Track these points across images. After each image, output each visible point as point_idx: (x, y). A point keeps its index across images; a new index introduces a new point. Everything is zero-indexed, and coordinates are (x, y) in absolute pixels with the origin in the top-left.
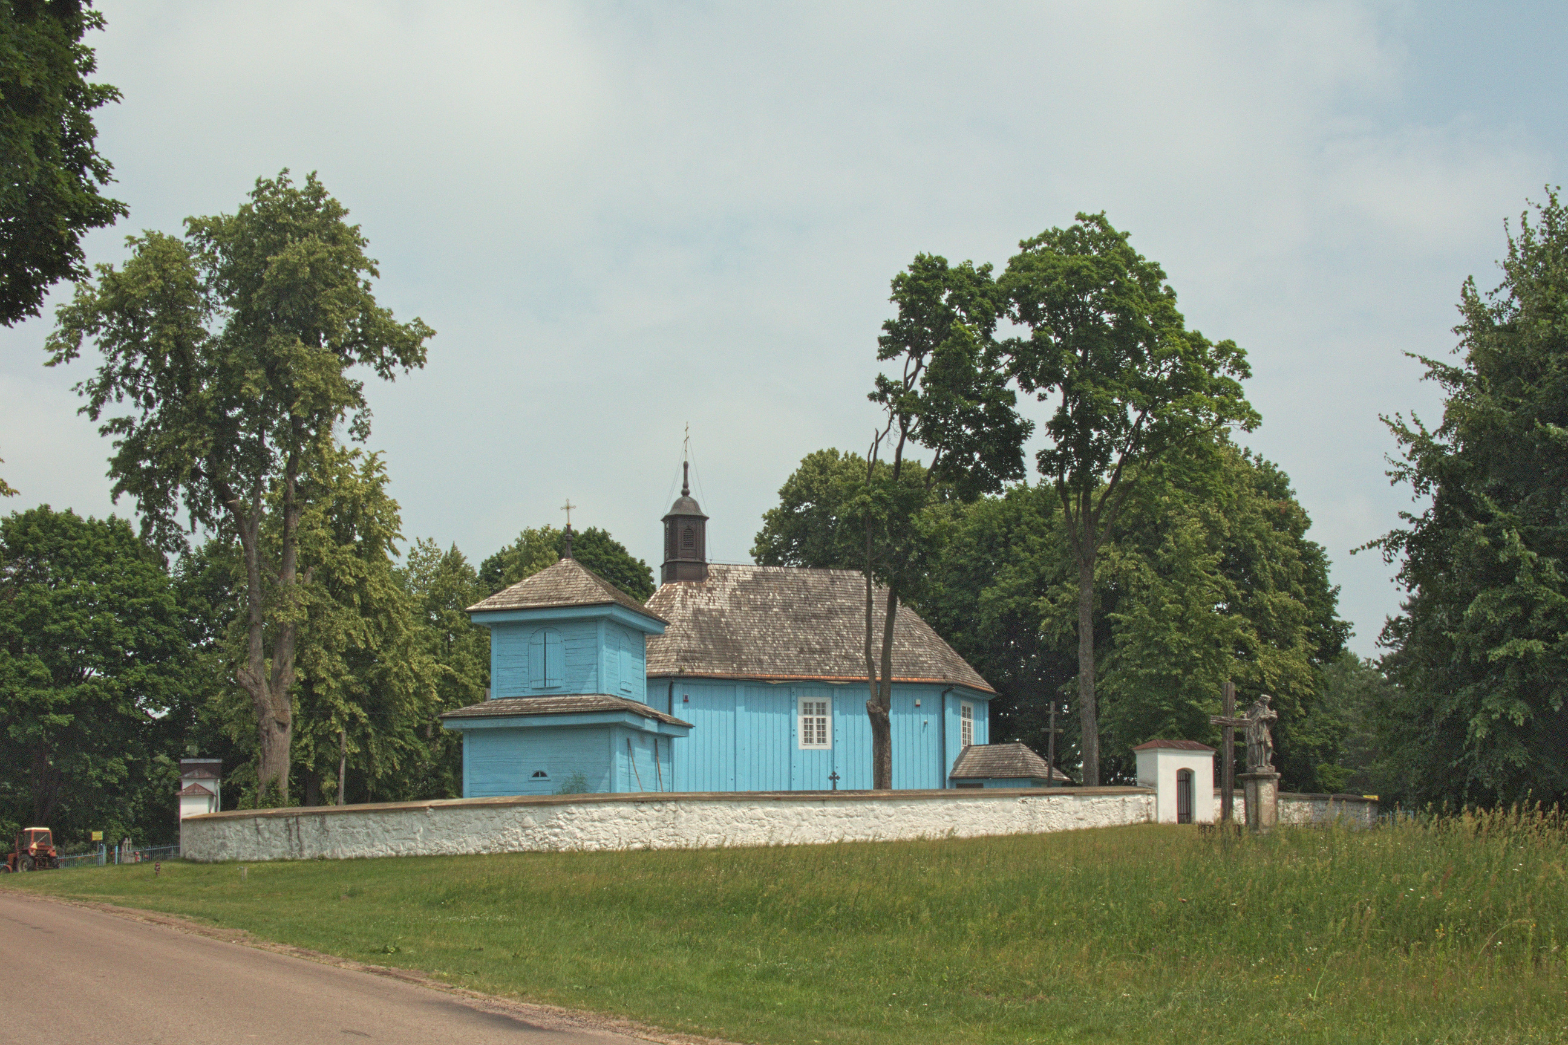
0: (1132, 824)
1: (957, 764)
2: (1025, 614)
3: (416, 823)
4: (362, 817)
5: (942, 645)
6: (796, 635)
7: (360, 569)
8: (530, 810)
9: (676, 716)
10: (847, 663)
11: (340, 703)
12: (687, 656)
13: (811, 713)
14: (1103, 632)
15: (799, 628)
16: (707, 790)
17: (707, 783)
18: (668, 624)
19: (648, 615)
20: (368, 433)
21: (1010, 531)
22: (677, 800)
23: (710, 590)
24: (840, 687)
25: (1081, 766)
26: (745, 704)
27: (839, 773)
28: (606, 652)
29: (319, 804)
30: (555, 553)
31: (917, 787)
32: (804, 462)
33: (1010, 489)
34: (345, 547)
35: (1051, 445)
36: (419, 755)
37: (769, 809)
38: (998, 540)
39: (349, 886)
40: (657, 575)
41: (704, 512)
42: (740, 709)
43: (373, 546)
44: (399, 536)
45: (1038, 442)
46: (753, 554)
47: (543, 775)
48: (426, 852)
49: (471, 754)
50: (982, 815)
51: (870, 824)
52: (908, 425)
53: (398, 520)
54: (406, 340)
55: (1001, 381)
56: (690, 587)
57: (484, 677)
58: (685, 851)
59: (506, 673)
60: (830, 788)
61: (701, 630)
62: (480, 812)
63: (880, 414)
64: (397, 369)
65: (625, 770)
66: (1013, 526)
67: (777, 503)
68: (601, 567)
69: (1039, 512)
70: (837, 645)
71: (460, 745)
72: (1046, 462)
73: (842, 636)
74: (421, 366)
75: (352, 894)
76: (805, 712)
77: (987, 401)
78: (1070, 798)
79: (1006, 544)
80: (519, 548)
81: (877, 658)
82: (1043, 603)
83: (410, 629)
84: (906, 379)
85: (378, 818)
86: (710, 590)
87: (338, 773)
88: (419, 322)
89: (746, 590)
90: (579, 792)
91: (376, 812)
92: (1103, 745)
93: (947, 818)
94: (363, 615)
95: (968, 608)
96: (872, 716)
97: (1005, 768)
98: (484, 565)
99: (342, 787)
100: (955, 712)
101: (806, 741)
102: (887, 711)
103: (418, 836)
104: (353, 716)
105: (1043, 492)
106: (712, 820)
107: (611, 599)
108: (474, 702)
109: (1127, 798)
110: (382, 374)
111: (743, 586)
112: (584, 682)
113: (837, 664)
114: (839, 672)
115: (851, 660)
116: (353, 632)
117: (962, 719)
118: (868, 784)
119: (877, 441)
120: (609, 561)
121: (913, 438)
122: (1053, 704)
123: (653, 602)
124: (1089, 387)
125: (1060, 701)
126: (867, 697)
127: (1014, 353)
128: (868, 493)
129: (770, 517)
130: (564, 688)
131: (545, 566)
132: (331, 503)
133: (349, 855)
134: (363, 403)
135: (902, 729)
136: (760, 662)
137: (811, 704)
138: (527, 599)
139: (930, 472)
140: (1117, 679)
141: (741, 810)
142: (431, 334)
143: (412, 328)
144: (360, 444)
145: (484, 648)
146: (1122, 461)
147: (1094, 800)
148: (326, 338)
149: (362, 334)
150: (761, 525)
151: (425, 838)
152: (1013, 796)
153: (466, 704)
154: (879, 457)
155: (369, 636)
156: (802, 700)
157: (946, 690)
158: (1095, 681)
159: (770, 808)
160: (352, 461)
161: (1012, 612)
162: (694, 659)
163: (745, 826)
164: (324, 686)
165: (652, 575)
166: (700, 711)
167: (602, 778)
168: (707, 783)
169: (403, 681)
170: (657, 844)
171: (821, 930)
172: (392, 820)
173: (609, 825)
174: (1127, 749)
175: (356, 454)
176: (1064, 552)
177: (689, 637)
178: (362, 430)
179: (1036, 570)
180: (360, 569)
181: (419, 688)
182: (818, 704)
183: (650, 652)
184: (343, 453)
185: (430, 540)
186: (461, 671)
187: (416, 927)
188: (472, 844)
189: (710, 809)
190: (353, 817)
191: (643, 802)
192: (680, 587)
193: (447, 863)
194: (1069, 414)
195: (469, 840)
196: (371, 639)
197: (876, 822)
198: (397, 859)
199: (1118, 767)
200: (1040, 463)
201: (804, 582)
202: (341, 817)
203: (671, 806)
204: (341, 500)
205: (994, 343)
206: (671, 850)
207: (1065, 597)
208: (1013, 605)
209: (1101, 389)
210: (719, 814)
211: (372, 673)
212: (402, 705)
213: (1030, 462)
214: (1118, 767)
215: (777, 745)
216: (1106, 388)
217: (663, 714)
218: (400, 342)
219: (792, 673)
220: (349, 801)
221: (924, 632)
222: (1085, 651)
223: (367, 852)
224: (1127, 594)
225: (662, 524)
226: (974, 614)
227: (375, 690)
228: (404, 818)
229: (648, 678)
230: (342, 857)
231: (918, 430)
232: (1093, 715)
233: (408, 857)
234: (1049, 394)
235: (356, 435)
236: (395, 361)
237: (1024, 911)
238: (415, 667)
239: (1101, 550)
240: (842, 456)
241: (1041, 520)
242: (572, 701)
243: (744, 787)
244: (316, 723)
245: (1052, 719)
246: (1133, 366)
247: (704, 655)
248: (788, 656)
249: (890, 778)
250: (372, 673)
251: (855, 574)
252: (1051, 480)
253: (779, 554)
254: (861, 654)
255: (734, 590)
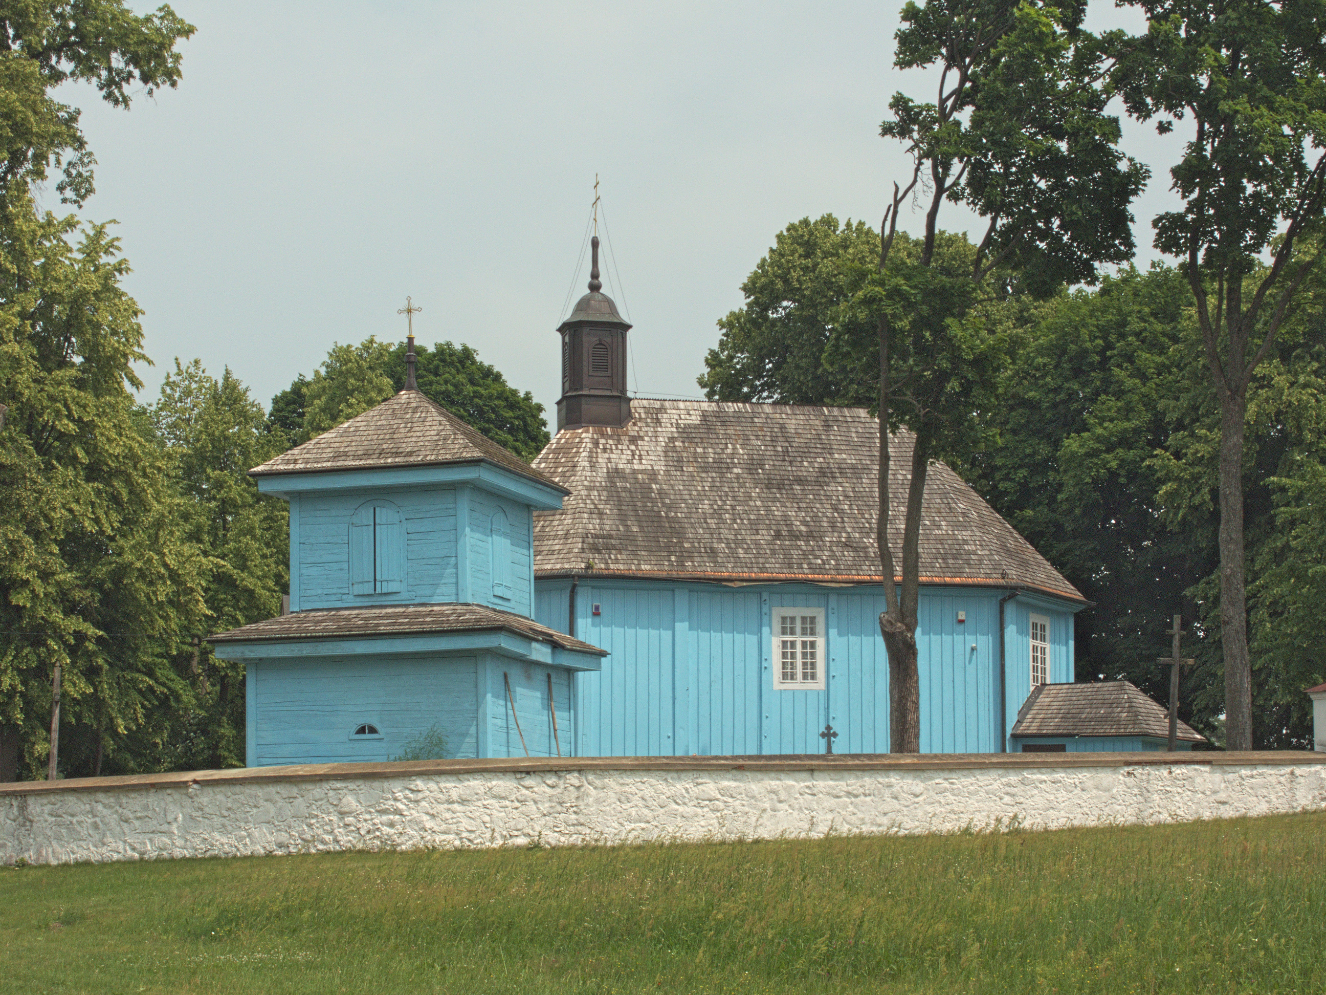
0: (1305, 812)
1: (1023, 714)
2: (1133, 476)
3: (171, 807)
4: (85, 798)
5: (999, 526)
6: (768, 510)
7: (85, 407)
8: (352, 786)
9: (581, 637)
10: (849, 554)
11: (57, 616)
12: (597, 544)
13: (793, 633)
14: (1258, 502)
15: (775, 500)
16: (630, 753)
17: (630, 743)
18: (567, 493)
19: (537, 480)
20: (90, 191)
21: (1109, 346)
22: (581, 770)
23: (634, 440)
24: (839, 592)
25: (1223, 717)
26: (690, 619)
27: (835, 728)
28: (471, 538)
29: (19, 778)
30: (387, 381)
31: (960, 750)
32: (780, 237)
33: (1106, 278)
34: (59, 374)
35: (1177, 204)
36: (178, 699)
37: (725, 783)
38: (1087, 361)
39: (62, 907)
40: (550, 416)
41: (625, 316)
42: (682, 627)
43: (105, 370)
44: (143, 357)
45: (1157, 199)
46: (703, 385)
47: (373, 730)
48: (187, 854)
49: (259, 699)
50: (1063, 795)
51: (886, 808)
52: (946, 174)
53: (138, 332)
54: (146, 41)
55: (1096, 102)
56: (603, 435)
57: (278, 577)
58: (595, 848)
59: (314, 571)
60: (823, 751)
61: (620, 503)
62: (272, 789)
63: (900, 158)
64: (134, 88)
65: (501, 722)
66: (1113, 338)
67: (740, 303)
68: (463, 405)
69: (1154, 314)
70: (833, 526)
71: (243, 683)
72: (1170, 232)
73: (842, 512)
74: (174, 84)
75: (69, 921)
76: (784, 633)
77: (1073, 137)
78: (1207, 768)
79: (1104, 364)
80: (329, 377)
81: (896, 545)
82: (1161, 459)
83: (163, 500)
84: (943, 101)
85: (111, 800)
86: (634, 440)
87: (49, 730)
88: (166, 12)
89: (691, 440)
90: (431, 758)
91: (107, 790)
92: (1259, 685)
93: (1007, 799)
94: (88, 480)
95: (1041, 467)
96: (889, 638)
97: (1103, 720)
98: (276, 401)
99: (55, 751)
100: (1020, 632)
101: (784, 676)
102: (913, 631)
103: (174, 828)
104: (80, 637)
105: (1160, 279)
106: (636, 800)
107: (477, 454)
108: (269, 615)
109: (1299, 770)
110: (109, 96)
111: (686, 433)
112: (435, 585)
113: (833, 556)
114: (837, 568)
115: (855, 549)
116: (74, 506)
117: (1032, 642)
118: (882, 743)
119: (897, 202)
120: (477, 395)
121: (955, 197)
122: (1177, 620)
123: (545, 459)
124: (1242, 105)
125: (1191, 614)
126: (880, 608)
127: (1120, 57)
128: (882, 284)
129: (731, 324)
130: (405, 595)
131: (371, 403)
132: (33, 303)
133: (64, 858)
134: (80, 143)
135: (936, 658)
136: (713, 553)
137: (793, 619)
138: (346, 454)
139: (981, 253)
140: (1281, 579)
141: (681, 785)
142: (188, 31)
143: (157, 21)
144: (72, 208)
145: (279, 531)
146: (1292, 231)
147: (1245, 772)
148: (17, 37)
149: (76, 31)
150: (714, 338)
151: (185, 830)
152: (1114, 765)
153: (250, 620)
154: (899, 228)
155: (101, 513)
156: (778, 613)
157: (1006, 596)
158: (1246, 583)
159: (728, 783)
160: (64, 237)
161: (1113, 475)
162: (609, 548)
163: (688, 810)
164: (27, 593)
165: (543, 415)
166: (618, 631)
167: (464, 735)
168: (630, 743)
169: (151, 583)
170: (551, 838)
171: (804, 975)
172: (134, 803)
173: (476, 809)
174: (1298, 692)
175: (70, 224)
176: (1197, 378)
177: (601, 514)
178: (79, 186)
179: (1149, 404)
180: (85, 407)
181: (177, 594)
182: (804, 619)
183: (539, 538)
184: (50, 223)
185: (197, 362)
186: (243, 568)
187: (167, 971)
188: (259, 839)
189: (633, 784)
190: (71, 799)
191: (528, 772)
192: (587, 435)
193: (220, 869)
194: (1208, 154)
195: (256, 833)
196: (103, 517)
197: (895, 804)
198: (142, 864)
199: (1284, 719)
200: (1159, 235)
201: (783, 427)
202: (52, 798)
203: (573, 779)
204: (50, 299)
205: (1089, 37)
206: (572, 847)
207: (1203, 450)
208: (1114, 464)
209: (1264, 110)
210: (648, 792)
211: (101, 571)
212: (152, 622)
213: (1143, 233)
214: (1284, 719)
215: (739, 683)
216: (1271, 108)
217: (560, 634)
218: (139, 43)
219: (763, 570)
220: (70, 774)
221: (972, 505)
222: (1231, 531)
223: (94, 853)
224: (1299, 442)
225: (559, 336)
226: (1051, 475)
227: (107, 599)
228: (152, 799)
229: (537, 578)
230: (54, 862)
231: (963, 181)
232: (1243, 637)
233: (159, 861)
234: (1175, 121)
235: (69, 193)
236: (130, 75)
237: (1125, 948)
238: (171, 561)
239: (1259, 370)
240: (842, 227)
241: (1159, 327)
242: (418, 615)
243: (689, 745)
244: (18, 650)
245: (1176, 642)
246: (1314, 73)
247: (625, 543)
248: (757, 543)
249: (917, 736)
250: (101, 571)
251: (862, 413)
252: (1173, 261)
253: (745, 382)
254: (871, 541)
255: (672, 439)
